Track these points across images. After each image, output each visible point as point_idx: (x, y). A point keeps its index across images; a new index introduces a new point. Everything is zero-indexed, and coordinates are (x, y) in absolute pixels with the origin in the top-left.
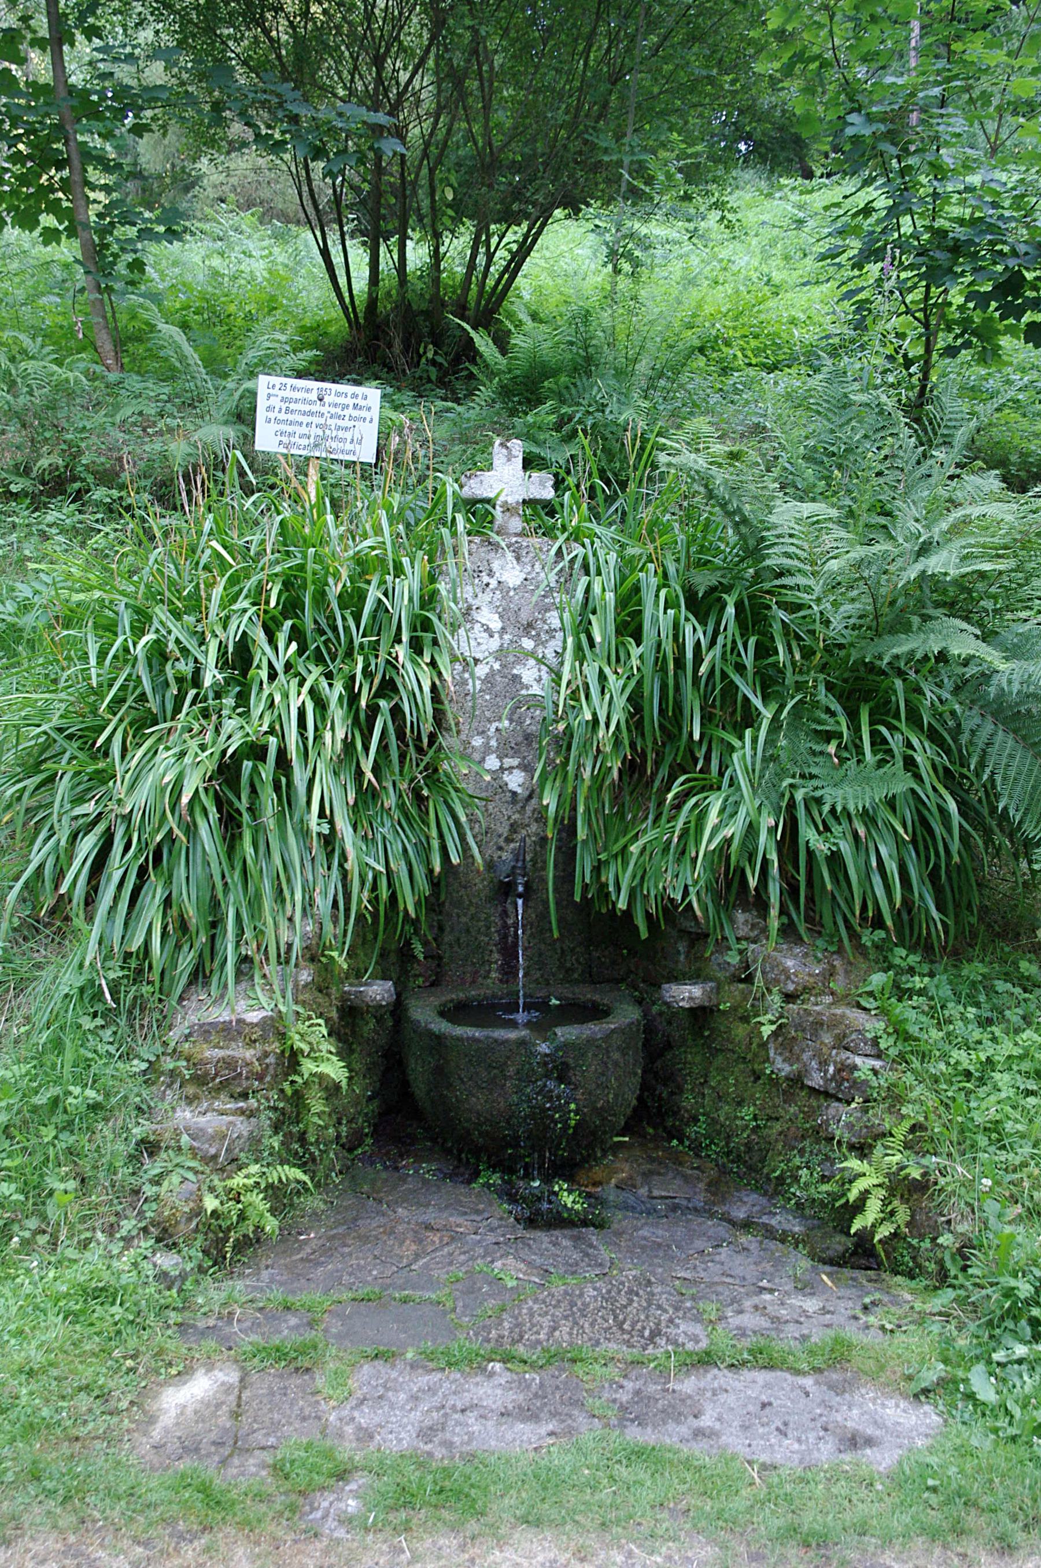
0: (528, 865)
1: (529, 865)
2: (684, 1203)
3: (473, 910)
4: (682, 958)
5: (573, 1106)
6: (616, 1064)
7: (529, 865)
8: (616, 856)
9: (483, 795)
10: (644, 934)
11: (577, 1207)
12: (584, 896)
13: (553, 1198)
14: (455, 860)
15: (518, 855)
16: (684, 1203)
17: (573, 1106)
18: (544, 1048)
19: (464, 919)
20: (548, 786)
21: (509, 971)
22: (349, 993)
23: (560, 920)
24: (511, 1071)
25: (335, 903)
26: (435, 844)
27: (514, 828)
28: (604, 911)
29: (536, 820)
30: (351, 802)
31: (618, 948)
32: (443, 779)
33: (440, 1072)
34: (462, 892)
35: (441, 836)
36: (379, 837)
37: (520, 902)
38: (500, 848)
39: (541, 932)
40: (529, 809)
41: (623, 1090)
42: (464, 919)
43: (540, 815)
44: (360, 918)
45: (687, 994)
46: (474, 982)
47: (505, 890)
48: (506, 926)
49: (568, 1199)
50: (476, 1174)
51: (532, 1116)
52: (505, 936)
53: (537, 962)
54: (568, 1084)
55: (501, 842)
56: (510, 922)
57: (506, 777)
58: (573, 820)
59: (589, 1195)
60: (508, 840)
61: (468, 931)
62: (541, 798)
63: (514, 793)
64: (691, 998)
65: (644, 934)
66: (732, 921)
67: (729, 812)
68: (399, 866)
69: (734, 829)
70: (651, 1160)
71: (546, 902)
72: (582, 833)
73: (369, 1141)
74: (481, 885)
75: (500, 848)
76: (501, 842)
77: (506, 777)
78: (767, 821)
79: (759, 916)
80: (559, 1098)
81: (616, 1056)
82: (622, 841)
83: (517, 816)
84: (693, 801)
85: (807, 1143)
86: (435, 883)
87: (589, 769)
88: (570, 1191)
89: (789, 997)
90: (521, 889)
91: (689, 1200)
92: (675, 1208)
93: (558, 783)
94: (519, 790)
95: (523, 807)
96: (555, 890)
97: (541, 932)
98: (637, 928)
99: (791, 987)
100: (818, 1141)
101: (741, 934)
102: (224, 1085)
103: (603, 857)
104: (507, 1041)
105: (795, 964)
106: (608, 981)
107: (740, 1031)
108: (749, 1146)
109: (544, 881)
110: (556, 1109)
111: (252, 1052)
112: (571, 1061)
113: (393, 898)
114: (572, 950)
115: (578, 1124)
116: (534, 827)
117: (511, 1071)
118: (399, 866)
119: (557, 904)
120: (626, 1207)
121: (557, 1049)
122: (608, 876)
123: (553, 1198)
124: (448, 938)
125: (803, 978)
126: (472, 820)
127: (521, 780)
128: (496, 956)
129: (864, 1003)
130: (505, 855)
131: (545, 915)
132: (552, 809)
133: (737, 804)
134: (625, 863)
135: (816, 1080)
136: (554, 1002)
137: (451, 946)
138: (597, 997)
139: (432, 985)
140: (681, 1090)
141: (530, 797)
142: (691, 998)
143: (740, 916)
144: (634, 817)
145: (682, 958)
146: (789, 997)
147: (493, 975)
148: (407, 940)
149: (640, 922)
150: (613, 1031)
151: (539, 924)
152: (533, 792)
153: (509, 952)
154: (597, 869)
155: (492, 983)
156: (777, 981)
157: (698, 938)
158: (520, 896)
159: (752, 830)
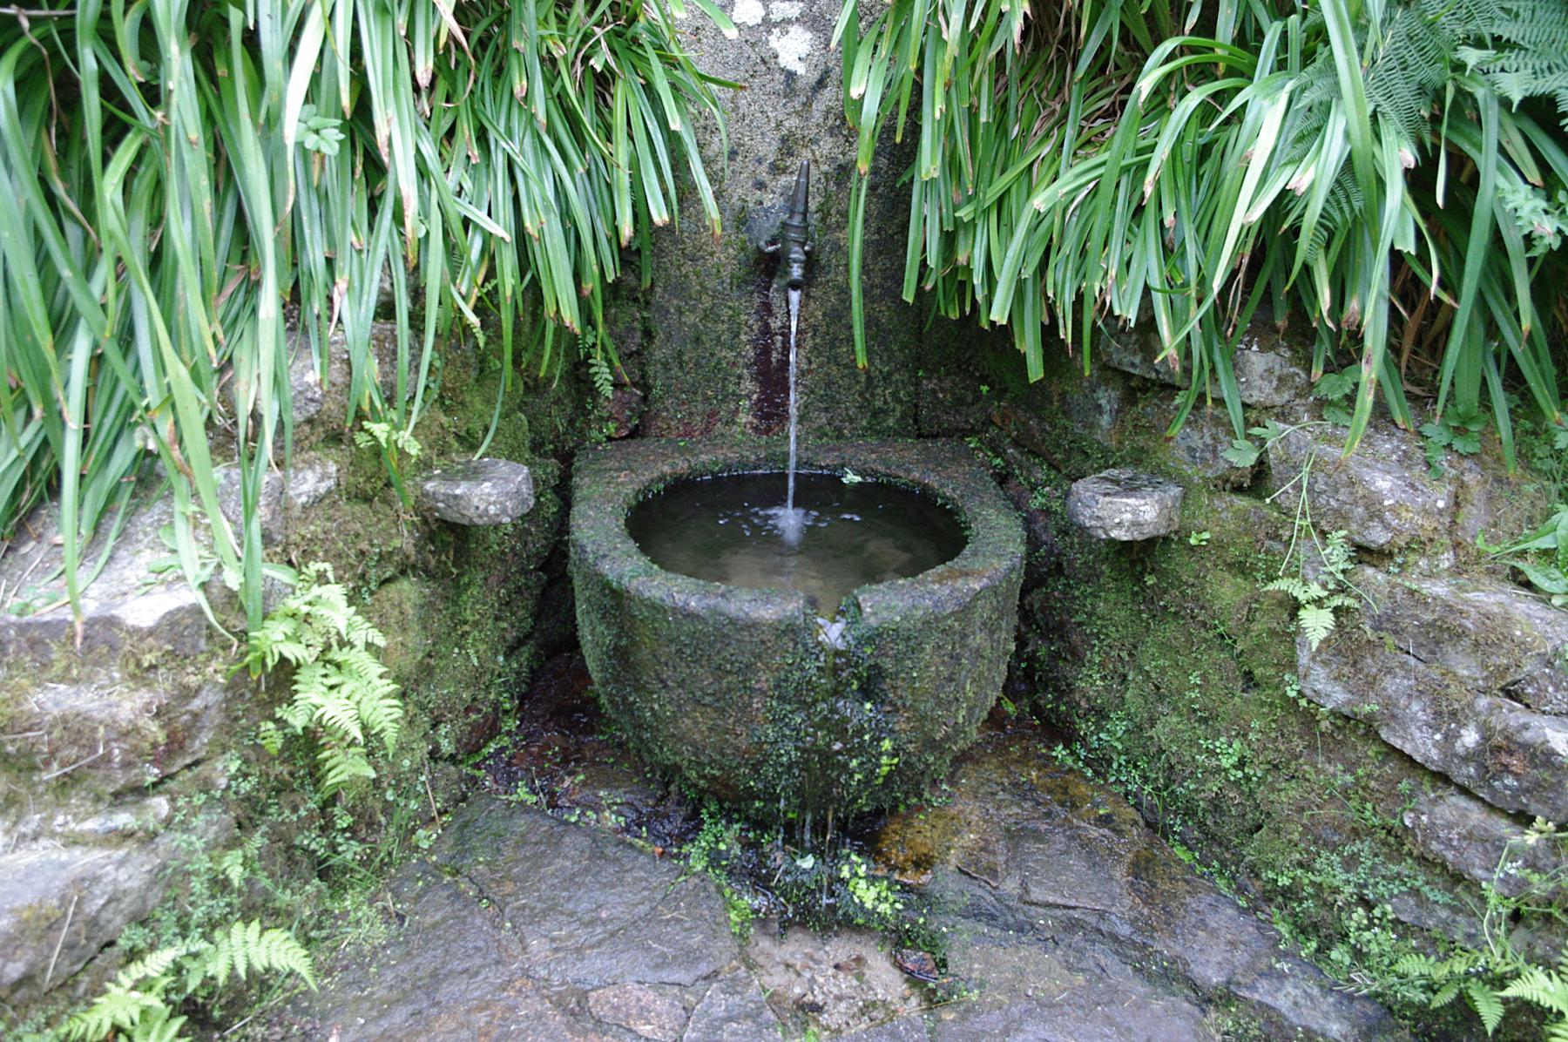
0: (813, 222)
1: (814, 219)
2: (1093, 920)
3: (707, 302)
4: (1105, 420)
5: (887, 745)
6: (978, 654)
7: (814, 219)
8: (987, 212)
9: (730, 76)
10: (1036, 372)
11: (884, 908)
12: (920, 291)
13: (837, 887)
14: (660, 215)
15: (796, 201)
16: (1093, 920)
17: (887, 745)
18: (833, 633)
19: (690, 319)
20: (863, 57)
21: (771, 413)
22: (434, 496)
23: (870, 322)
24: (764, 680)
25: (386, 310)
26: (623, 179)
27: (788, 146)
28: (954, 315)
29: (832, 131)
30: (424, 79)
31: (979, 393)
32: (645, 38)
33: (622, 656)
34: (688, 268)
35: (634, 165)
36: (499, 162)
37: (795, 296)
38: (761, 186)
39: (833, 342)
40: (818, 108)
41: (982, 685)
42: (690, 319)
43: (843, 124)
44: (454, 332)
45: (1124, 512)
46: (707, 430)
47: (768, 266)
48: (766, 330)
49: (866, 894)
50: (693, 826)
51: (805, 765)
52: (766, 351)
53: (825, 397)
54: (880, 702)
55: (763, 173)
56: (775, 324)
57: (775, 41)
58: (914, 130)
59: (906, 889)
60: (776, 170)
61: (697, 340)
62: (844, 83)
63: (791, 76)
64: (1136, 524)
65: (1036, 372)
66: (1236, 367)
67: (1306, 132)
68: (543, 223)
69: (1313, 176)
70: (1021, 792)
71: (845, 291)
72: (929, 163)
73: (511, 724)
74: (725, 259)
75: (761, 186)
76: (763, 173)
77: (775, 41)
78: (1399, 155)
79: (1295, 361)
80: (860, 732)
81: (978, 639)
82: (1000, 184)
83: (793, 122)
84: (1196, 96)
85: (1363, 847)
86: (627, 256)
87: (957, 18)
88: (872, 879)
89: (1364, 553)
90: (797, 272)
91: (1102, 915)
92: (1072, 926)
93: (884, 50)
94: (800, 69)
95: (807, 105)
96: (865, 269)
97: (833, 342)
98: (1021, 359)
99: (1378, 536)
100: (1396, 855)
101: (1256, 397)
102: (68, 783)
103: (965, 213)
104: (753, 626)
105: (1393, 484)
106: (948, 434)
107: (1227, 592)
108: (1216, 805)
109: (840, 250)
110: (851, 753)
111: (143, 696)
112: (888, 664)
113: (534, 293)
114: (887, 378)
115: (897, 771)
116: (827, 145)
117: (764, 680)
118: (543, 223)
119: (866, 292)
120: (974, 913)
121: (862, 641)
122: (972, 253)
123: (837, 887)
124: (660, 352)
125: (1411, 521)
126: (705, 129)
127: (804, 49)
128: (748, 385)
129: (1535, 577)
130: (769, 199)
131: (839, 315)
132: (871, 108)
133: (1325, 108)
134: (1006, 228)
135: (1423, 744)
136: (851, 478)
137: (666, 366)
138: (932, 480)
139: (633, 434)
140: (1077, 658)
141: (821, 84)
142: (1136, 524)
143: (1258, 361)
144: (1024, 134)
145: (1105, 420)
146: (1364, 553)
147: (743, 418)
148: (564, 370)
149: (1029, 344)
150: (977, 596)
151: (830, 332)
152: (827, 72)
153: (772, 379)
154: (949, 240)
155: (734, 444)
156: (1341, 518)
157: (1147, 390)
158: (795, 285)
159: (1354, 175)
